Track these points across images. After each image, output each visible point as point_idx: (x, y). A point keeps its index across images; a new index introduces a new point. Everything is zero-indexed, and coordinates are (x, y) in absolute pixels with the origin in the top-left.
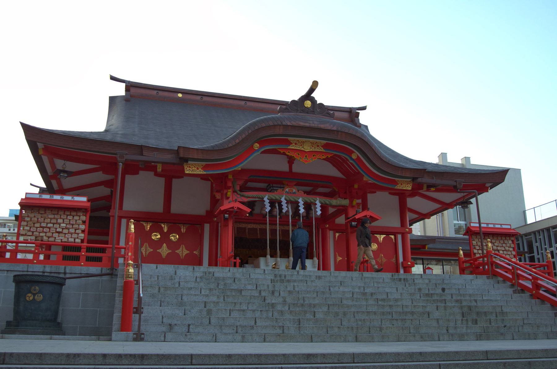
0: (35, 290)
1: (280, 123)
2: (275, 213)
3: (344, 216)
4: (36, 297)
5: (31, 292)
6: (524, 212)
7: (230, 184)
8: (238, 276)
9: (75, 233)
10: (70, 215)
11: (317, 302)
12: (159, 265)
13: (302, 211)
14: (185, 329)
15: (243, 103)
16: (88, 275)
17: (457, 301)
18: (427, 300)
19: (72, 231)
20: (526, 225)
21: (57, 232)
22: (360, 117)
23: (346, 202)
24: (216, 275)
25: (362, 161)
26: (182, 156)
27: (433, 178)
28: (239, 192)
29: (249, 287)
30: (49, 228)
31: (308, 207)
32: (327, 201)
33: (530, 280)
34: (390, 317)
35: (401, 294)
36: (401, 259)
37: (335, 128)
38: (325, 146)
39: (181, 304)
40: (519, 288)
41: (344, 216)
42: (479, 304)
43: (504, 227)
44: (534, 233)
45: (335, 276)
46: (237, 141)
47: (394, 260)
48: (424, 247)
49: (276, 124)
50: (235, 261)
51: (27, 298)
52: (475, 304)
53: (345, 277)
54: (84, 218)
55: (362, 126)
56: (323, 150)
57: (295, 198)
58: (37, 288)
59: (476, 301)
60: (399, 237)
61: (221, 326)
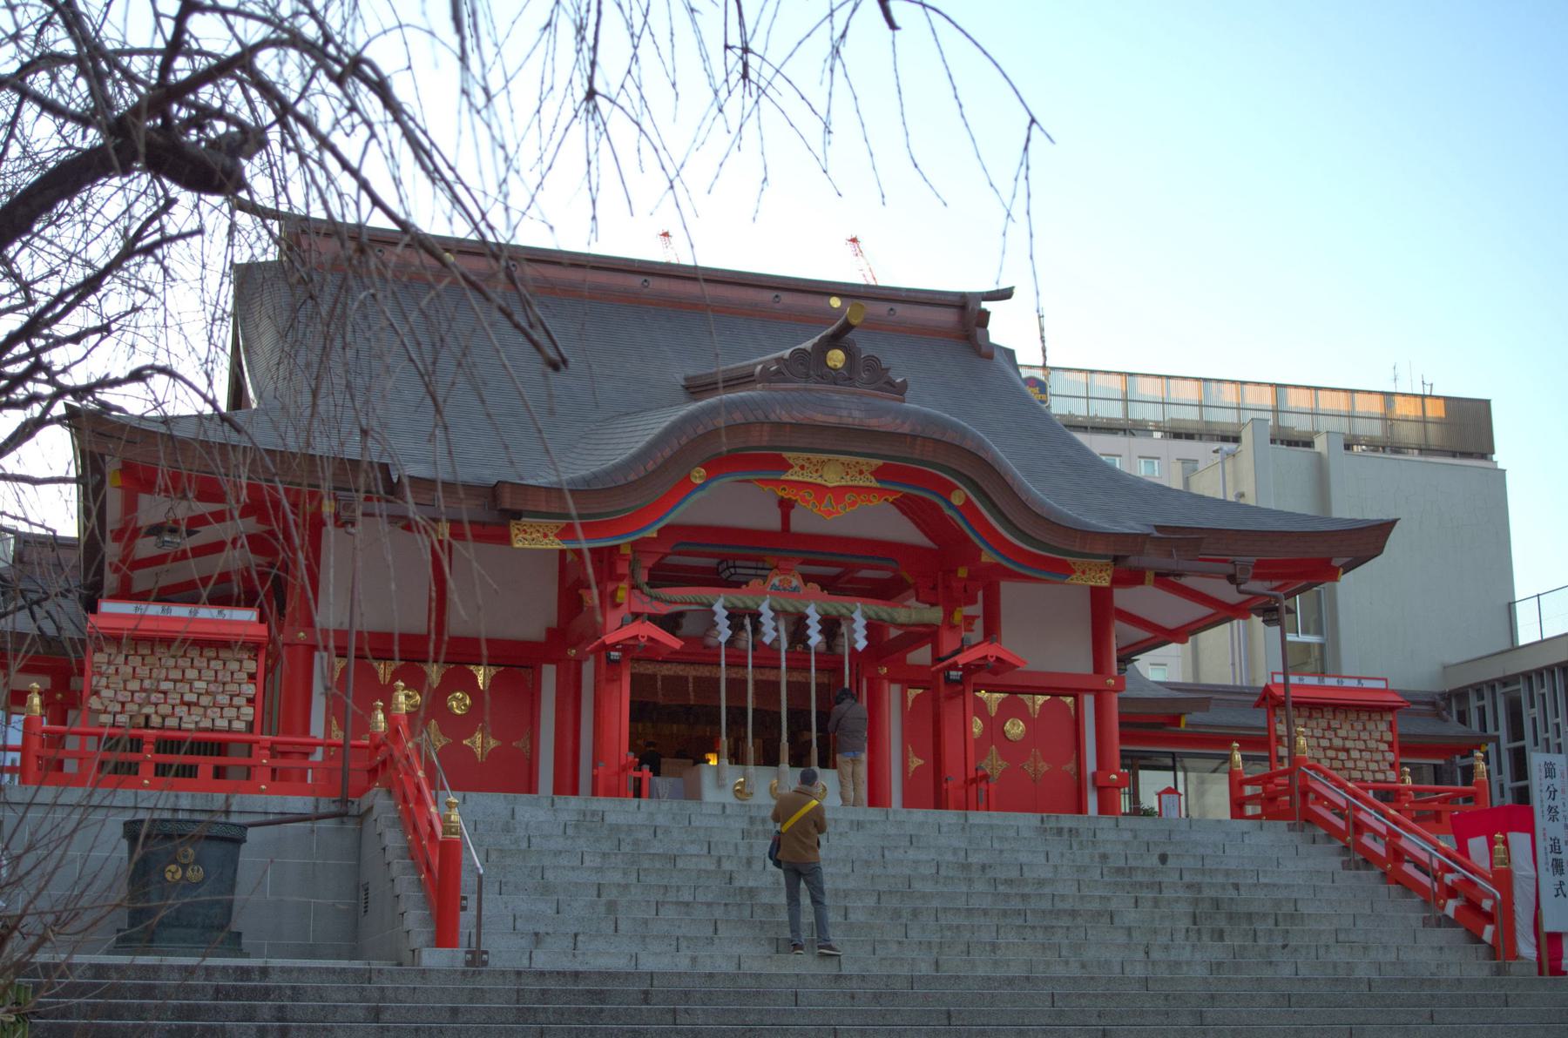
0: (186, 857)
1: (762, 418)
2: (741, 644)
3: (928, 648)
4: (189, 873)
5: (175, 861)
6: (1510, 607)
7: (623, 568)
8: (660, 820)
9: (231, 705)
10: (217, 658)
11: (851, 884)
12: (468, 794)
13: (815, 638)
14: (569, 942)
15: (636, 281)
16: (284, 819)
17: (1189, 886)
18: (1116, 884)
19: (223, 699)
20: (1514, 648)
21: (183, 703)
22: (992, 328)
23: (934, 615)
24: (611, 818)
25: (977, 510)
26: (507, 506)
27: (1170, 555)
28: (646, 589)
29: (692, 849)
30: (165, 693)
31: (831, 626)
32: (881, 610)
33: (1382, 836)
34: (1020, 922)
35: (1055, 867)
36: (1091, 765)
37: (906, 429)
38: (878, 473)
39: (546, 889)
40: (1359, 857)
41: (928, 648)
42: (1244, 894)
43: (1367, 684)
44: (1528, 676)
45: (900, 818)
46: (651, 466)
47: (1070, 767)
48: (1176, 720)
49: (752, 419)
50: (638, 774)
51: (169, 876)
52: (1234, 894)
53: (922, 824)
54: (251, 666)
55: (996, 354)
56: (875, 484)
57: (798, 605)
58: (190, 851)
59: (1236, 887)
60: (1089, 701)
61: (644, 938)
